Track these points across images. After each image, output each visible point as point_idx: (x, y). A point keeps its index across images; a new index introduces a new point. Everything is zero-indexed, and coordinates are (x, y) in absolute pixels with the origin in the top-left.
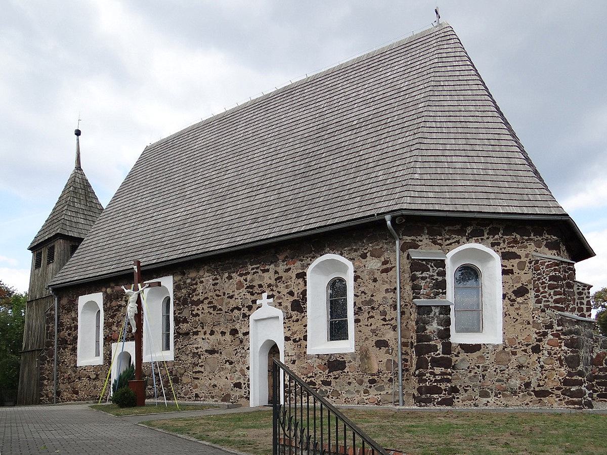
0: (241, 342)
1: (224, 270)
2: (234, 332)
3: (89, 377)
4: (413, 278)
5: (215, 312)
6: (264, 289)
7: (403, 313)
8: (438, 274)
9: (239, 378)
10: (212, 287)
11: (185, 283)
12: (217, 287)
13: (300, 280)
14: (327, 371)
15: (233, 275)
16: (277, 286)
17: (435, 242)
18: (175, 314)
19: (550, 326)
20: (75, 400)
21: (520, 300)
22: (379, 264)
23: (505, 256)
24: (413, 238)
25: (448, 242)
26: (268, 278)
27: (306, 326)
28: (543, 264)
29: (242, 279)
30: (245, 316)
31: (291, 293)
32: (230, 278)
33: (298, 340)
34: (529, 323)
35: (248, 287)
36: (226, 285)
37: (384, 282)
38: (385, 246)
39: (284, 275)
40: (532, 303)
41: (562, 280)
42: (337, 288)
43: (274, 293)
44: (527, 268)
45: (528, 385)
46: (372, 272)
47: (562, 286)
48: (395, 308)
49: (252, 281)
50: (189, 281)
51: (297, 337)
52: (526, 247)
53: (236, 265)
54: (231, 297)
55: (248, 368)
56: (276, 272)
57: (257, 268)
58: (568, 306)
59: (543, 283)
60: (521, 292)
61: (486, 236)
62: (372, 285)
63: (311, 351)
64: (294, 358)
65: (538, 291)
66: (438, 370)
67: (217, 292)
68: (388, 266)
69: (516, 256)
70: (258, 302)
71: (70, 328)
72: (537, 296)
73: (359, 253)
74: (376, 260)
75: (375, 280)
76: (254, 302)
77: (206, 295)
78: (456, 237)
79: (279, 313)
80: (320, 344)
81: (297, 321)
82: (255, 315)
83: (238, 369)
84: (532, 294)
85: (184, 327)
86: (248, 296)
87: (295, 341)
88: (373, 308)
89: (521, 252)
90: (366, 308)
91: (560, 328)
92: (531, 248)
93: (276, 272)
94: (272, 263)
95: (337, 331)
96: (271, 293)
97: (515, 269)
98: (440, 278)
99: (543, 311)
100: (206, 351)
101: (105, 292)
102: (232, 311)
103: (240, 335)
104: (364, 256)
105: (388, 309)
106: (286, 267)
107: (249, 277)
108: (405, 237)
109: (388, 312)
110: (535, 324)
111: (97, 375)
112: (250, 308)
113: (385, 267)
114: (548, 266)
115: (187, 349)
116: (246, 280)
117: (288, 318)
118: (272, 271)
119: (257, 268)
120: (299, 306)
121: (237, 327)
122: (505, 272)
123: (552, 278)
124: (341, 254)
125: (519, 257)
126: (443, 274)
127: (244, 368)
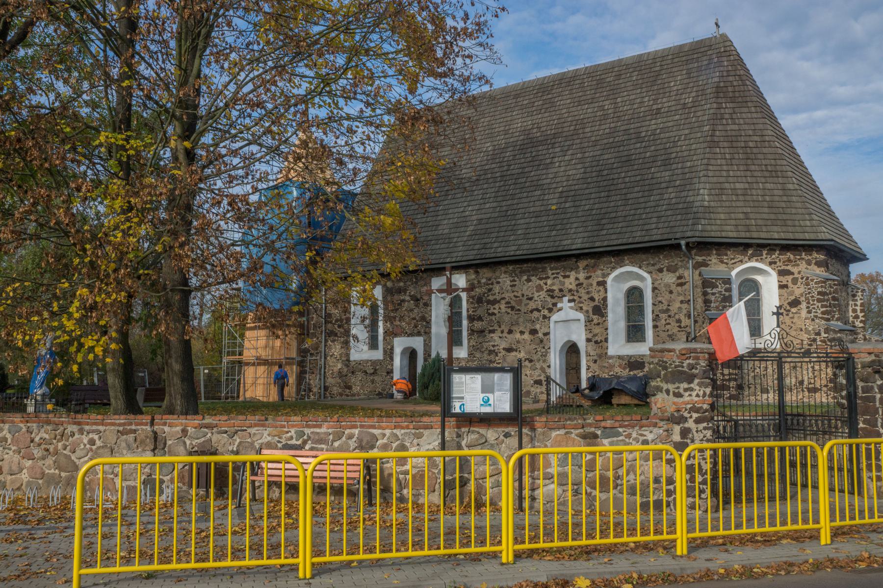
0: (542, 341)
1: (522, 272)
2: (534, 332)
3: (366, 372)
4: (705, 294)
5: (513, 312)
6: (564, 293)
7: (696, 322)
8: (726, 290)
9: (540, 376)
10: (509, 288)
11: (479, 282)
12: (516, 289)
13: (601, 288)
14: (628, 370)
15: (533, 278)
16: (578, 291)
17: (722, 262)
18: (468, 311)
19: (818, 334)
20: (347, 396)
21: (794, 310)
22: (675, 279)
23: (782, 273)
24: (704, 258)
25: (733, 261)
26: (570, 283)
27: (607, 329)
28: (812, 280)
29: (542, 283)
30: (545, 317)
31: (592, 299)
32: (529, 280)
33: (599, 342)
34: (801, 330)
35: (548, 291)
36: (525, 288)
37: (679, 294)
38: (680, 263)
39: (585, 282)
40: (804, 313)
41: (828, 295)
42: (634, 296)
43: (575, 298)
44: (799, 283)
45: (801, 383)
46: (667, 285)
47: (828, 300)
48: (689, 317)
49: (553, 284)
50: (484, 281)
51: (598, 338)
52: (798, 265)
53: (535, 269)
54: (531, 299)
55: (549, 367)
56: (577, 279)
57: (558, 273)
58: (833, 316)
59: (813, 297)
60: (795, 303)
61: (765, 256)
62: (667, 296)
63: (611, 352)
64: (595, 358)
65: (808, 303)
66: (726, 371)
67: (516, 294)
68: (683, 280)
69: (789, 273)
70: (559, 305)
71: (341, 320)
72: (808, 307)
73: (657, 267)
74: (671, 275)
75: (671, 292)
76: (555, 305)
77: (503, 296)
78: (740, 257)
79: (581, 316)
80: (618, 346)
81: (598, 324)
82: (555, 317)
83: (538, 366)
84: (804, 305)
85: (478, 325)
86: (549, 299)
87: (596, 342)
88: (669, 316)
89: (795, 270)
90: (663, 316)
91: (826, 335)
92: (803, 266)
93: (577, 279)
94: (572, 269)
95: (635, 332)
96: (571, 298)
97: (790, 284)
98: (727, 294)
99: (813, 320)
100: (504, 349)
101: (385, 286)
102: (532, 312)
103: (540, 335)
104: (661, 270)
105: (682, 318)
106: (586, 275)
107: (549, 282)
108: (697, 257)
109: (683, 321)
110: (807, 332)
111: (376, 370)
112: (550, 310)
113: (680, 281)
114: (816, 283)
115: (483, 347)
116: (546, 284)
117: (589, 321)
118: (572, 279)
119: (558, 273)
120: (600, 310)
121: (538, 327)
122: (782, 287)
123: (819, 293)
124: (640, 267)
125: (793, 274)
126: (729, 290)
127: (545, 366)
